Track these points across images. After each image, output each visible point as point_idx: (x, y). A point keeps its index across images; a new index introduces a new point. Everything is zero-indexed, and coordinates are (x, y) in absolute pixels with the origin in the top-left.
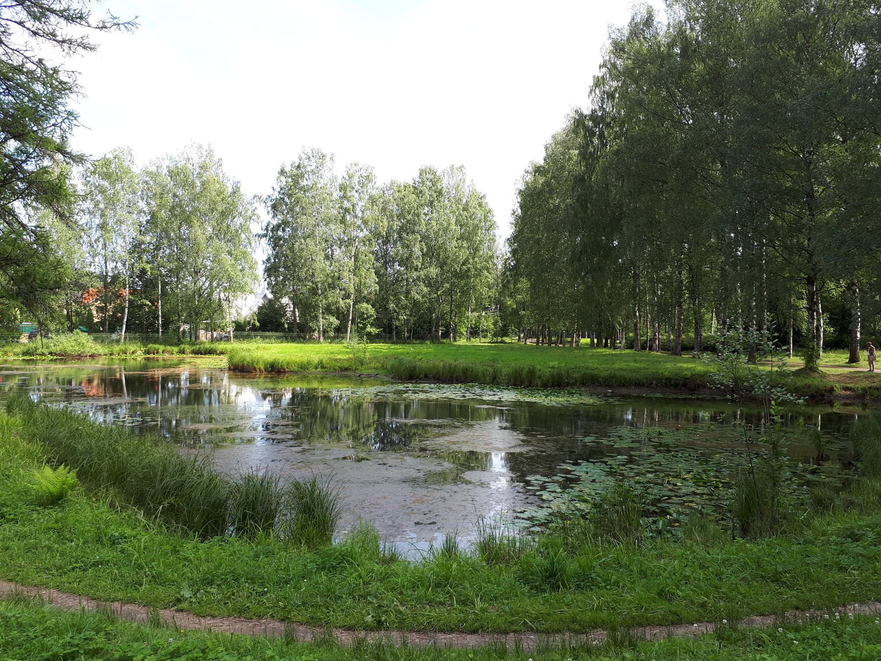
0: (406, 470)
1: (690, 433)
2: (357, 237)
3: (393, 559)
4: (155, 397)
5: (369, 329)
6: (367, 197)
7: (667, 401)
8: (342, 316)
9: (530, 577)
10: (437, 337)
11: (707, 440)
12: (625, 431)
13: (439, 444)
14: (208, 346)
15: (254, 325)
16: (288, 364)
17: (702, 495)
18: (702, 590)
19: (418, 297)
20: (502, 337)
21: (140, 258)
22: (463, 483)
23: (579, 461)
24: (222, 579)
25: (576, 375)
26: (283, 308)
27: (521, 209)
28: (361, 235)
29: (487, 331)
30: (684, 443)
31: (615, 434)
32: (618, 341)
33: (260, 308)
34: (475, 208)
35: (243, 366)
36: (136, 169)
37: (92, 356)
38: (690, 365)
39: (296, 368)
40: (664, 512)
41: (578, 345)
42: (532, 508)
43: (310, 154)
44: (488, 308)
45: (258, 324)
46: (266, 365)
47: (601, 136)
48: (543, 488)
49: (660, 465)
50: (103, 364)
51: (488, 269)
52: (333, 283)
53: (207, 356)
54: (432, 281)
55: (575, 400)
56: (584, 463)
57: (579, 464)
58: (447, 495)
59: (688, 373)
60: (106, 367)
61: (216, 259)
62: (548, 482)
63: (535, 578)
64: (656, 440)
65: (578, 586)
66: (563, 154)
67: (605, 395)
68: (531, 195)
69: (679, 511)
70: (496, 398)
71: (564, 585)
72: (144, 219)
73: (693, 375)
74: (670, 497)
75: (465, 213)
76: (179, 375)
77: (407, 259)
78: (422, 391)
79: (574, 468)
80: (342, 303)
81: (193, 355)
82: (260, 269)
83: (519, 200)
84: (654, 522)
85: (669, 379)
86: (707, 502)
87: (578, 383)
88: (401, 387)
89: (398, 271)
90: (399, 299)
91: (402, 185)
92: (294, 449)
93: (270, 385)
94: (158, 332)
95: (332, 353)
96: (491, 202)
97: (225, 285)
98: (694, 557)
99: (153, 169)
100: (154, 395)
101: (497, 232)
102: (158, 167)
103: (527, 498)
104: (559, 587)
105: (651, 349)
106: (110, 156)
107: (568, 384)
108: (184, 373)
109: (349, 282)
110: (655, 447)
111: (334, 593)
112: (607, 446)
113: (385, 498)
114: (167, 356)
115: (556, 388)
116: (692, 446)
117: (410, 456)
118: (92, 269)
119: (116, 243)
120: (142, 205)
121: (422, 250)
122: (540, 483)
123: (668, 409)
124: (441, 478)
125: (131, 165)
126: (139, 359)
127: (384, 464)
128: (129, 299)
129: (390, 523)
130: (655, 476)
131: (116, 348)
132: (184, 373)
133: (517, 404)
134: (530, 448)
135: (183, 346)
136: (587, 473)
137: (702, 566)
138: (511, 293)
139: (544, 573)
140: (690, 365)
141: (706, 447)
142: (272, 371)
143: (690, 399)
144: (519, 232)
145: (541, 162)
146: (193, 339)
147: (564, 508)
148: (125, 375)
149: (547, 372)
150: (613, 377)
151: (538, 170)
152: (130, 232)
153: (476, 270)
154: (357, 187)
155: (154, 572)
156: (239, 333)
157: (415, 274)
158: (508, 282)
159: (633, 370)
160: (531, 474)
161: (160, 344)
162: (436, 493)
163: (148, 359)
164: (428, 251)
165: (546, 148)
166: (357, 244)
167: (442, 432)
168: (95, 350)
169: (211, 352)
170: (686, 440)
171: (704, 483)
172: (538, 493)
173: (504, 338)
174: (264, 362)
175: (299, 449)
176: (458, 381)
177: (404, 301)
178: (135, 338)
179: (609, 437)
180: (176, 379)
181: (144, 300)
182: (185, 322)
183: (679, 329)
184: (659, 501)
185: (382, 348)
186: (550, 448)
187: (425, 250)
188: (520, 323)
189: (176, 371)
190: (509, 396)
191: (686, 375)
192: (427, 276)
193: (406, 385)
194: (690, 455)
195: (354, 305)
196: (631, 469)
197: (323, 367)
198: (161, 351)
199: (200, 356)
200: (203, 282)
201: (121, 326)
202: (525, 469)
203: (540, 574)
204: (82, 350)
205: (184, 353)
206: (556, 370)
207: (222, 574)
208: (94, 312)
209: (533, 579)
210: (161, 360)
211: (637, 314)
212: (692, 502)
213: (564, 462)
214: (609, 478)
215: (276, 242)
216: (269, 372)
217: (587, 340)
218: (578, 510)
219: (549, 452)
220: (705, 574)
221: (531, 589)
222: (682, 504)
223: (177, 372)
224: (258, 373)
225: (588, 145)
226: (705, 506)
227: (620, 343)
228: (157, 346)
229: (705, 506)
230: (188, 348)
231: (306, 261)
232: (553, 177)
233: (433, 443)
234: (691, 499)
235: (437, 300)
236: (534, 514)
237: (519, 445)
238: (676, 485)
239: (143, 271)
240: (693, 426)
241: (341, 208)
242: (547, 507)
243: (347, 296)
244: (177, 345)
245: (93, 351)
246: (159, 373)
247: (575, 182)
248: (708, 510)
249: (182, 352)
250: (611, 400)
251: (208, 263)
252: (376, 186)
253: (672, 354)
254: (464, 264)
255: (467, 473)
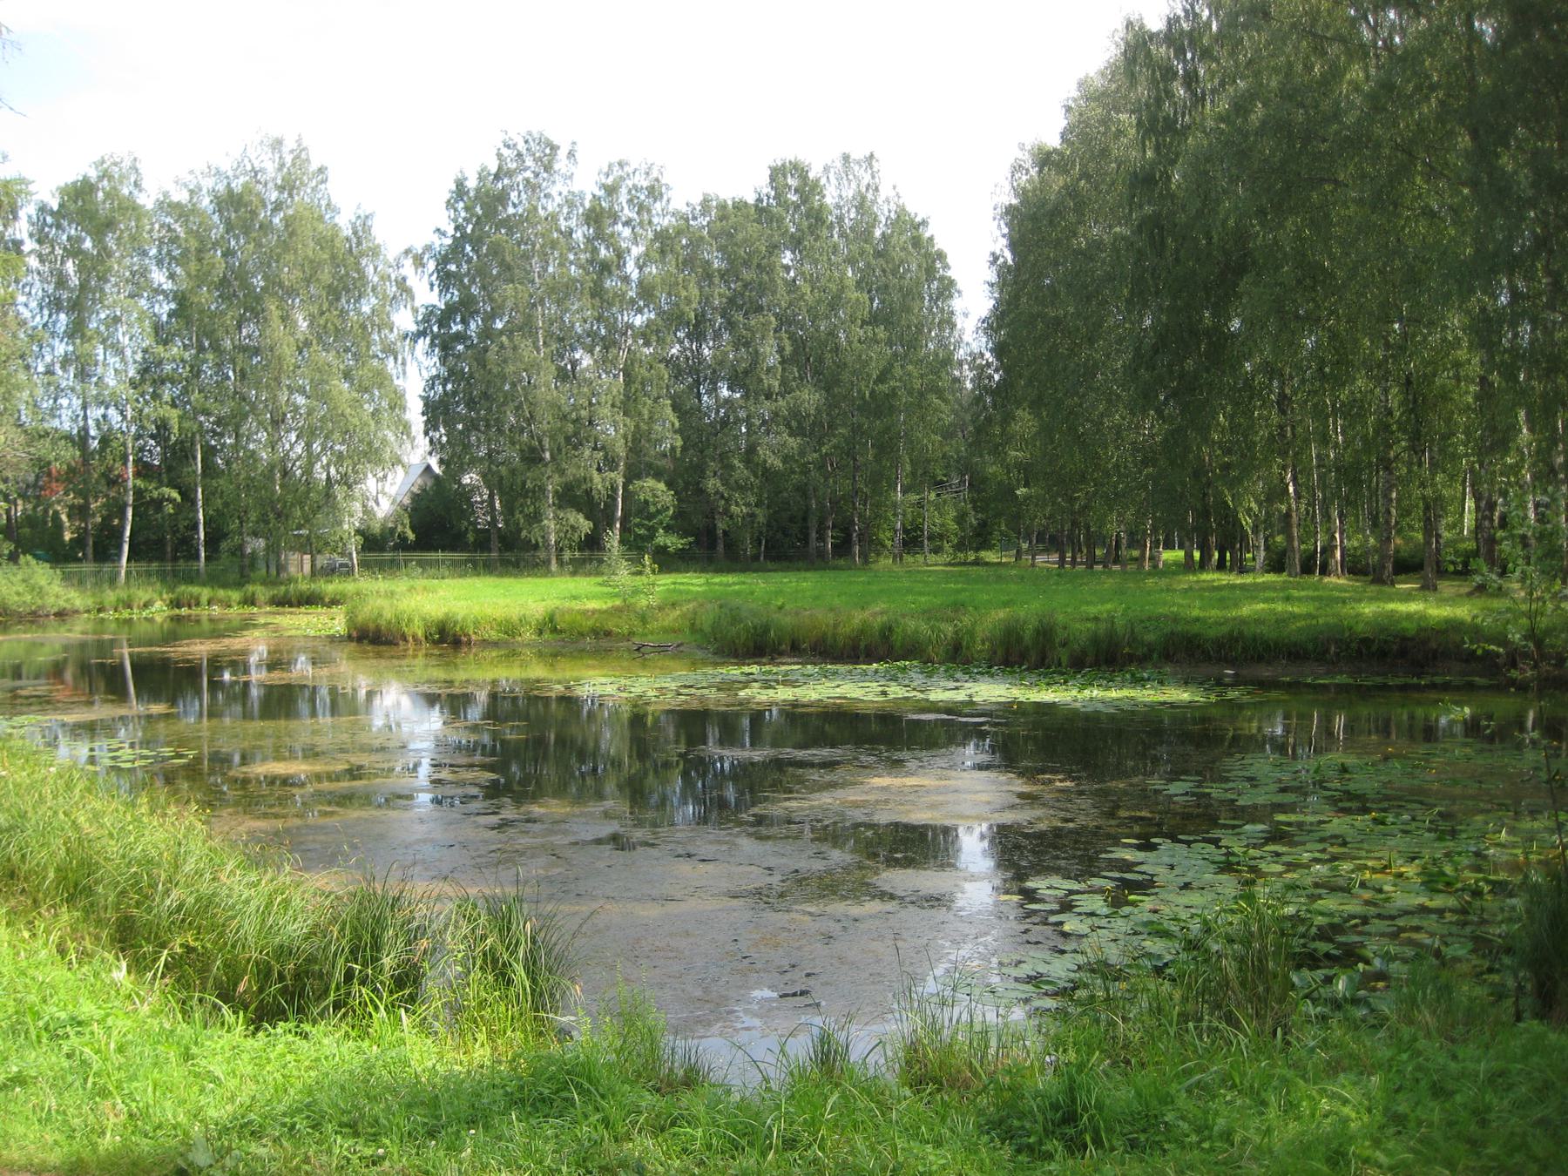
0: (741, 869)
1: (1415, 767)
2: (629, 326)
3: (692, 1079)
4: (197, 704)
5: (662, 538)
6: (651, 235)
7: (1364, 693)
8: (600, 514)
9: (1016, 1123)
10: (821, 554)
11: (1455, 782)
12: (1263, 764)
13: (820, 807)
14: (304, 586)
15: (403, 538)
16: (476, 623)
17: (1440, 912)
18: (1437, 1150)
19: (776, 462)
20: (977, 550)
21: (156, 396)
22: (873, 897)
23: (1153, 840)
24: (284, 1125)
25: (1150, 637)
26: (466, 494)
27: (1013, 252)
28: (638, 321)
29: (941, 537)
30: (1400, 789)
31: (1241, 774)
32: (1249, 556)
33: (416, 498)
34: (903, 249)
35: (378, 630)
36: (147, 200)
37: (61, 615)
38: (1414, 607)
39: (494, 635)
40: (1349, 957)
41: (1155, 567)
42: (1039, 954)
43: (522, 147)
44: (942, 482)
45: (411, 536)
46: (427, 627)
47: (1191, 79)
48: (1066, 906)
49: (1344, 844)
50: (83, 633)
51: (939, 393)
52: (577, 432)
53: (303, 609)
54: (807, 425)
55: (1148, 695)
56: (1165, 845)
57: (1153, 847)
58: (835, 928)
59: (1411, 628)
60: (90, 637)
61: (319, 393)
62: (1078, 892)
63: (1028, 1125)
64: (1336, 784)
65: (1133, 1145)
66: (1105, 122)
67: (1219, 683)
68: (1034, 218)
69: (1388, 952)
70: (961, 696)
71: (1098, 1142)
72: (164, 309)
73: (1421, 629)
74: (1365, 920)
75: (881, 261)
76: (245, 652)
77: (746, 372)
78: (785, 683)
79: (1140, 856)
80: (597, 477)
81: (274, 609)
82: (415, 414)
83: (1006, 231)
84: (1328, 980)
85: (1366, 642)
86: (1454, 929)
87: (1155, 656)
88: (734, 672)
89: (727, 401)
90: (732, 467)
91: (730, 203)
92: (482, 820)
93: (440, 674)
94: (197, 557)
95: (575, 598)
96: (941, 235)
97: (337, 447)
98: (1419, 1068)
99: (182, 196)
100: (192, 702)
101: (957, 304)
102: (192, 192)
103: (1026, 931)
104: (1085, 1147)
105: (1325, 571)
106: (93, 175)
107: (1131, 658)
108: (257, 646)
109: (612, 430)
110: (1333, 801)
111: (541, 1163)
112: (1222, 802)
113: (687, 934)
114: (216, 610)
115: (1104, 668)
116: (1419, 796)
117: (750, 835)
118: (56, 423)
119: (105, 365)
120: (159, 277)
121: (781, 350)
122: (1060, 893)
123: (1364, 711)
124: (828, 887)
125: (136, 192)
126: (159, 619)
127: (689, 856)
128: (134, 486)
129: (698, 993)
130: (1332, 870)
131: (110, 596)
132: (257, 646)
133: (1011, 711)
134: (1039, 812)
135: (250, 588)
136: (1172, 867)
137: (1439, 1091)
138: (996, 447)
139: (1049, 1115)
140: (1414, 607)
141: (1453, 799)
142: (442, 640)
143: (1417, 688)
144: (1009, 303)
145: (1054, 141)
146: (273, 571)
147: (1113, 955)
148: (131, 655)
149: (1081, 630)
150: (1237, 641)
151: (1045, 159)
152: (133, 340)
153: (910, 393)
154: (628, 213)
155: (134, 1105)
156: (372, 556)
157: (766, 409)
158: (989, 420)
159: (1282, 620)
160: (1038, 873)
161: (204, 584)
162: (804, 915)
163: (177, 619)
164: (795, 352)
165: (1068, 109)
166: (630, 341)
167: (828, 778)
168: (67, 600)
169: (310, 600)
170: (1407, 782)
171: (1448, 884)
172: (1053, 919)
173: (983, 554)
174: (424, 619)
175: (494, 819)
176: (870, 655)
177: (741, 470)
178: (149, 574)
179: (1227, 780)
180: (239, 663)
181: (166, 490)
182: (255, 534)
183: (1387, 522)
184: (1336, 929)
185: (694, 582)
186: (1086, 814)
187: (788, 349)
188: (1017, 517)
189: (236, 643)
190: (991, 691)
191: (1404, 630)
192: (795, 413)
193: (746, 669)
194: (1414, 819)
195: (628, 481)
196: (1278, 854)
197: (554, 630)
198: (204, 599)
199: (287, 609)
200: (293, 445)
201: (120, 547)
202: (1024, 863)
203: (1040, 1118)
204: (40, 602)
205: (253, 603)
206: (1103, 626)
207: (284, 1115)
208: (64, 517)
209: (1023, 1128)
210: (204, 619)
211: (1291, 489)
212: (1417, 929)
213: (1117, 843)
214: (1223, 877)
215: (445, 345)
216: (435, 643)
217: (1179, 554)
218: (1149, 955)
219: (1082, 820)
220: (1443, 1110)
221: (1019, 1151)
222: (1394, 936)
223: (238, 647)
224: (411, 645)
225: (1159, 102)
226: (1449, 940)
227: (1254, 559)
228: (195, 590)
229: (1449, 940)
230: (261, 592)
231: (514, 385)
232: (1085, 175)
233: (806, 804)
234: (1415, 922)
235: (821, 467)
236: (1042, 969)
237: (1012, 807)
238: (1380, 891)
239: (163, 426)
240: (1422, 749)
241: (591, 262)
242: (1075, 951)
243: (610, 463)
244: (238, 585)
245: (62, 603)
246: (200, 649)
247: (1132, 186)
248: (1458, 950)
249: (250, 601)
250: (1232, 694)
251: (300, 400)
252: (671, 208)
253: (1373, 582)
254: (881, 379)
255: (884, 875)
